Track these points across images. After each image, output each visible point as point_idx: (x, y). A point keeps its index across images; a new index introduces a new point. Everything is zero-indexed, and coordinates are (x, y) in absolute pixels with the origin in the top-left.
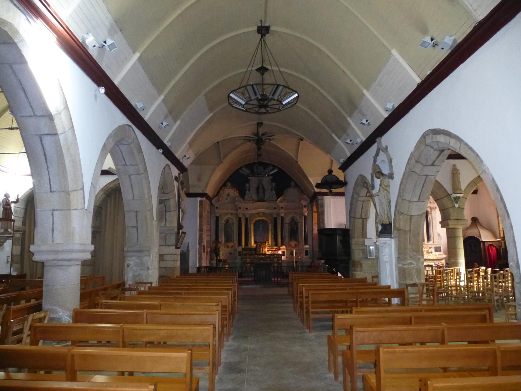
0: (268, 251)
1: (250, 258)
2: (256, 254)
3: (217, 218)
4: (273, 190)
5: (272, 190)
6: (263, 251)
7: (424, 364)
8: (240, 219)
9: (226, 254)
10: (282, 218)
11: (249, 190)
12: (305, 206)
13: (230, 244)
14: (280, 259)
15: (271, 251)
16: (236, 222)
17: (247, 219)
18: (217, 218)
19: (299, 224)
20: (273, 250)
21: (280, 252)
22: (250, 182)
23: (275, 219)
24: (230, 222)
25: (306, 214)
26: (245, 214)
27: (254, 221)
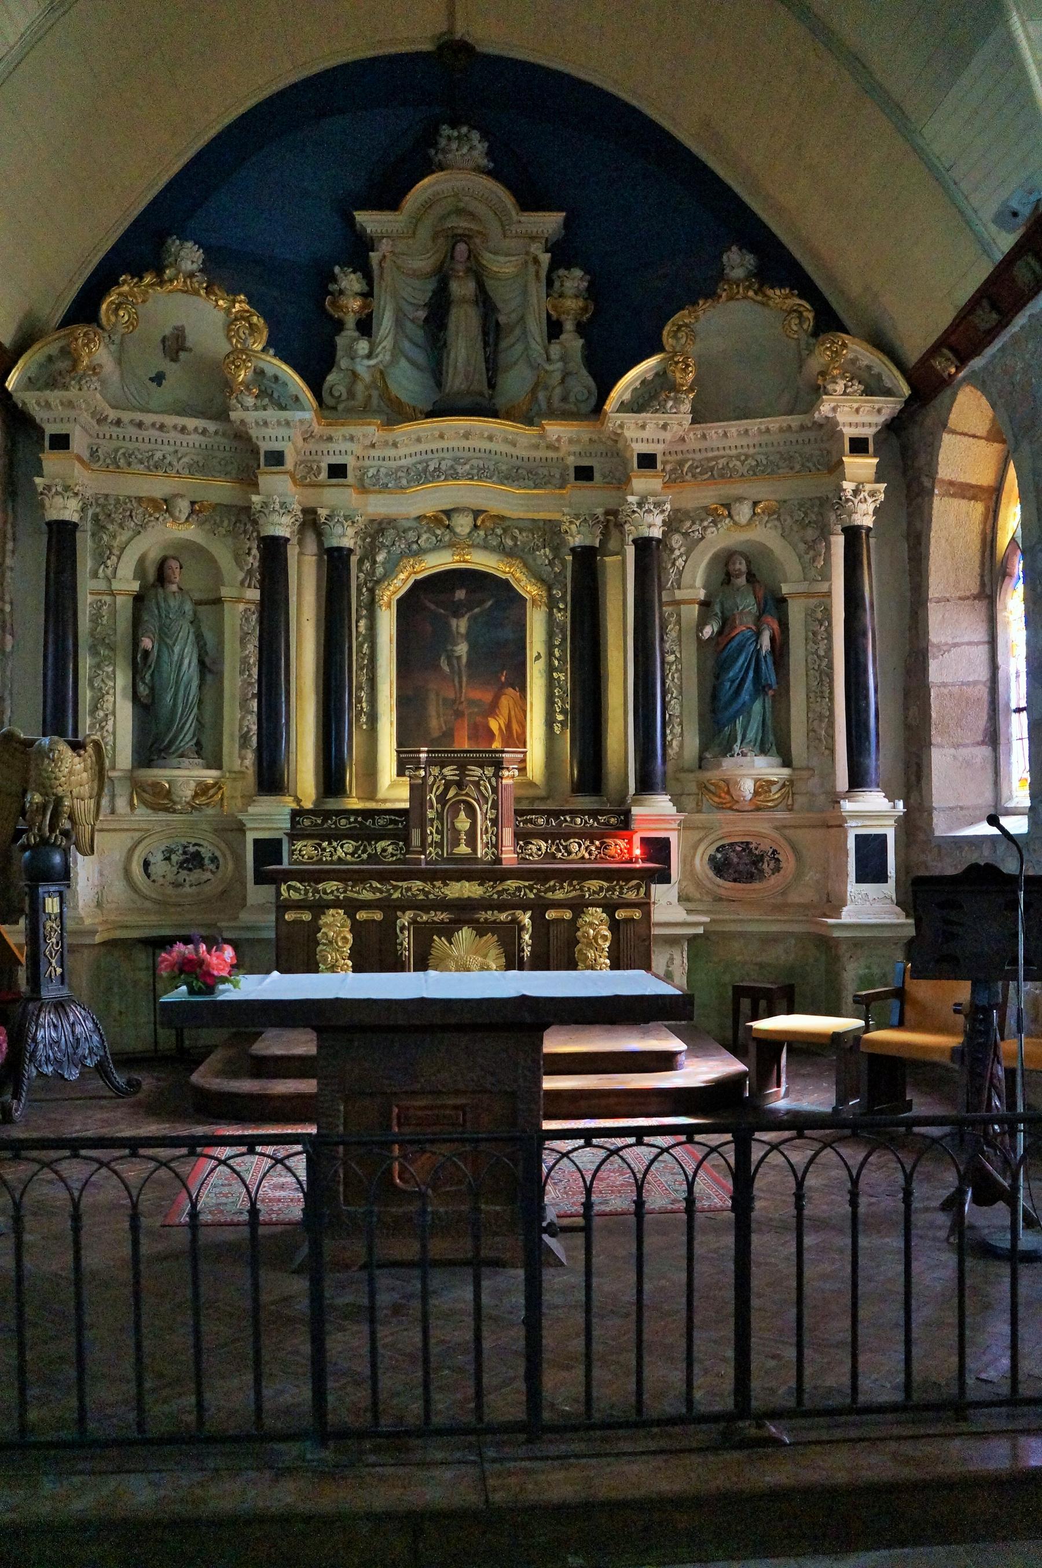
4: (569, 326)
6: (472, 842)
9: (146, 864)
14: (637, 914)
22: (374, 256)
27: (400, 584)
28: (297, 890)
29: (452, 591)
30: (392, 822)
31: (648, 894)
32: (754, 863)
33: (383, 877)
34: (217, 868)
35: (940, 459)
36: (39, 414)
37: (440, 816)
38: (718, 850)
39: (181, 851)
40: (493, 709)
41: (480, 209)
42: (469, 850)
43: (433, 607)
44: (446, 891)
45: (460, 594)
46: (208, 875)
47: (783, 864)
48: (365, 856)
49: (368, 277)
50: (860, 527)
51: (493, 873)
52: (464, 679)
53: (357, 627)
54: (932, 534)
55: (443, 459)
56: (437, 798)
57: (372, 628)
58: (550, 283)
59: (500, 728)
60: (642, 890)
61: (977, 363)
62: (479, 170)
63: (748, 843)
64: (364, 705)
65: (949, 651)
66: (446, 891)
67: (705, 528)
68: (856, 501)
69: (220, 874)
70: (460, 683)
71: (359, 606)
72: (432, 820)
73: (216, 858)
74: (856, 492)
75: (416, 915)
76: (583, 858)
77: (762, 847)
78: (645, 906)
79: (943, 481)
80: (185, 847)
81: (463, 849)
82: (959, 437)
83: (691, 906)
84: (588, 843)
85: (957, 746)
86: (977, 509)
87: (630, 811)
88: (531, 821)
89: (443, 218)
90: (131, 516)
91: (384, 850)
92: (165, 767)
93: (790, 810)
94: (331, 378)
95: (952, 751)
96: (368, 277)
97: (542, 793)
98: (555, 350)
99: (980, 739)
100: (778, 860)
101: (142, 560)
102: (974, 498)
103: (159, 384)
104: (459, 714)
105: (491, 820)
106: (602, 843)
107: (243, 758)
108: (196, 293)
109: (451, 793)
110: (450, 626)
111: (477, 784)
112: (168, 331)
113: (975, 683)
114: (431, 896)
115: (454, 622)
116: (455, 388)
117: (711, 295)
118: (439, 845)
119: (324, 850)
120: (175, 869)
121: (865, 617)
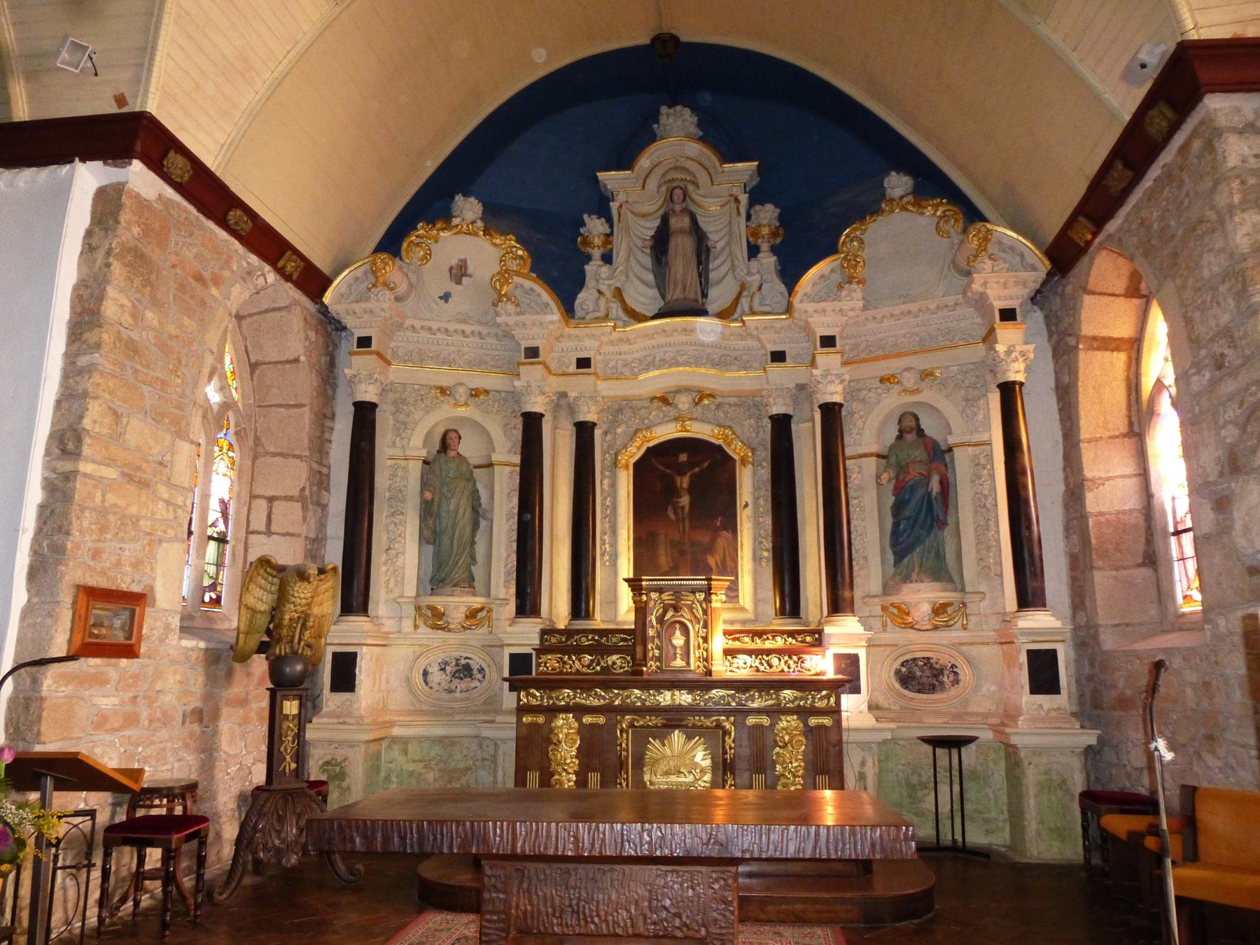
0: (729, 653)
1: (579, 710)
2: (636, 678)
3: (365, 415)
4: (765, 247)
5: (753, 251)
6: (686, 655)
7: (738, 627)
8: (532, 423)
9: (425, 673)
10: (831, 413)
11: (607, 259)
12: (1008, 315)
13: (457, 604)
14: (826, 721)
15: (750, 652)
16: (507, 453)
17: (584, 432)
18: (365, 415)
19: (962, 460)
20: (768, 645)
21: (821, 665)
22: (614, 206)
23: (782, 425)
24: (469, 448)
25: (1016, 372)
26: (572, 394)
27: (635, 452)
28: (534, 696)
29: (677, 456)
30: (623, 640)
31: (838, 702)
32: (935, 676)
33: (607, 686)
34: (484, 677)
35: (1082, 318)
36: (348, 321)
37: (659, 635)
38: (902, 665)
39: (454, 663)
40: (710, 549)
41: (690, 165)
42: (682, 663)
43: (661, 468)
44: (660, 698)
45: (683, 457)
46: (476, 683)
47: (961, 677)
48: (598, 668)
49: (609, 221)
50: (1014, 383)
51: (705, 683)
52: (687, 523)
53: (602, 484)
54: (1080, 383)
55: (667, 352)
56: (656, 618)
57: (613, 485)
58: (749, 218)
59: (717, 564)
60: (832, 700)
61: (1112, 227)
62: (690, 137)
63: (928, 658)
64: (607, 546)
65: (1103, 484)
66: (660, 698)
67: (880, 394)
68: (1009, 360)
69: (484, 684)
70: (684, 527)
71: (603, 469)
72: (653, 637)
73: (482, 669)
74: (1009, 353)
75: (633, 720)
76: (782, 671)
77: (941, 662)
78: (836, 712)
79: (1085, 337)
80: (457, 660)
81: (679, 663)
82: (1098, 297)
83: (879, 713)
84: (786, 658)
85: (1117, 569)
86: (1120, 359)
87: (823, 630)
88: (738, 639)
89: (667, 171)
90: (422, 400)
91: (614, 663)
92: (441, 595)
93: (965, 629)
94: (582, 296)
95: (1114, 573)
96: (609, 221)
97: (750, 616)
98: (754, 264)
99: (1140, 560)
100: (956, 673)
101: (429, 435)
102: (1117, 349)
103: (446, 301)
104: (682, 553)
105: (702, 637)
106: (799, 659)
107: (168, 512)
108: (476, 234)
109: (670, 614)
110: (675, 483)
111: (691, 608)
112: (454, 262)
113: (1131, 511)
114: (647, 703)
115: (678, 479)
116: (675, 297)
117: (877, 211)
118: (659, 659)
119: (565, 663)
120: (448, 678)
121: (1023, 459)
